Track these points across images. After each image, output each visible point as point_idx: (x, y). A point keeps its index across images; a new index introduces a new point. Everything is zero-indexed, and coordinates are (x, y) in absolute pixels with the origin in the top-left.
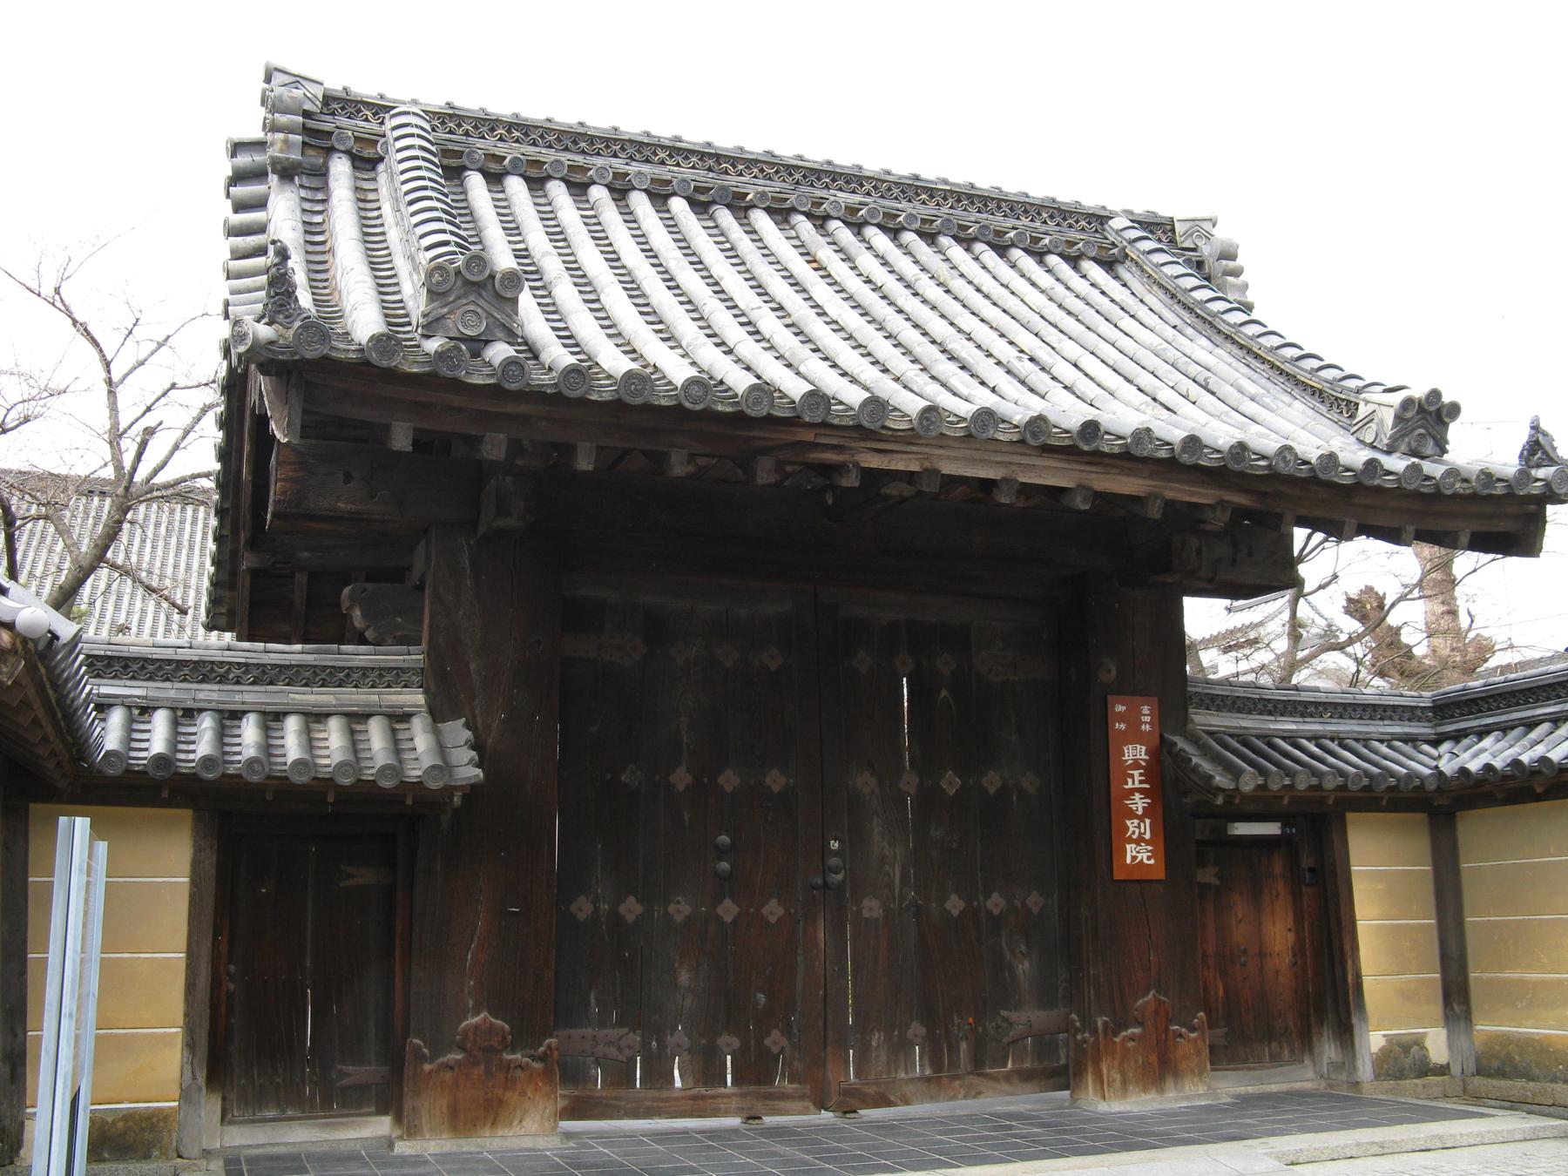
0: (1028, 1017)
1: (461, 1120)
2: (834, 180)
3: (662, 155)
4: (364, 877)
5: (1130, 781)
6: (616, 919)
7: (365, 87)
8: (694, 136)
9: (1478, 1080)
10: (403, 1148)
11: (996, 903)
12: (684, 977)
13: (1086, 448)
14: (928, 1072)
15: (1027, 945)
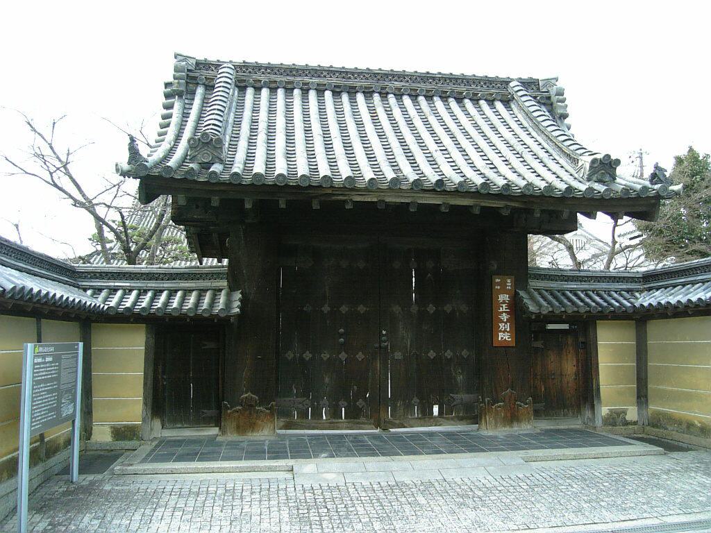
0: (462, 397)
1: (241, 429)
2: (393, 77)
3: (325, 73)
4: (211, 345)
5: (501, 308)
6: (302, 359)
7: (212, 58)
8: (338, 64)
9: (648, 428)
10: (219, 439)
11: (449, 354)
12: (327, 380)
13: (439, 190)
14: (420, 416)
15: (462, 370)
